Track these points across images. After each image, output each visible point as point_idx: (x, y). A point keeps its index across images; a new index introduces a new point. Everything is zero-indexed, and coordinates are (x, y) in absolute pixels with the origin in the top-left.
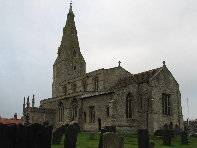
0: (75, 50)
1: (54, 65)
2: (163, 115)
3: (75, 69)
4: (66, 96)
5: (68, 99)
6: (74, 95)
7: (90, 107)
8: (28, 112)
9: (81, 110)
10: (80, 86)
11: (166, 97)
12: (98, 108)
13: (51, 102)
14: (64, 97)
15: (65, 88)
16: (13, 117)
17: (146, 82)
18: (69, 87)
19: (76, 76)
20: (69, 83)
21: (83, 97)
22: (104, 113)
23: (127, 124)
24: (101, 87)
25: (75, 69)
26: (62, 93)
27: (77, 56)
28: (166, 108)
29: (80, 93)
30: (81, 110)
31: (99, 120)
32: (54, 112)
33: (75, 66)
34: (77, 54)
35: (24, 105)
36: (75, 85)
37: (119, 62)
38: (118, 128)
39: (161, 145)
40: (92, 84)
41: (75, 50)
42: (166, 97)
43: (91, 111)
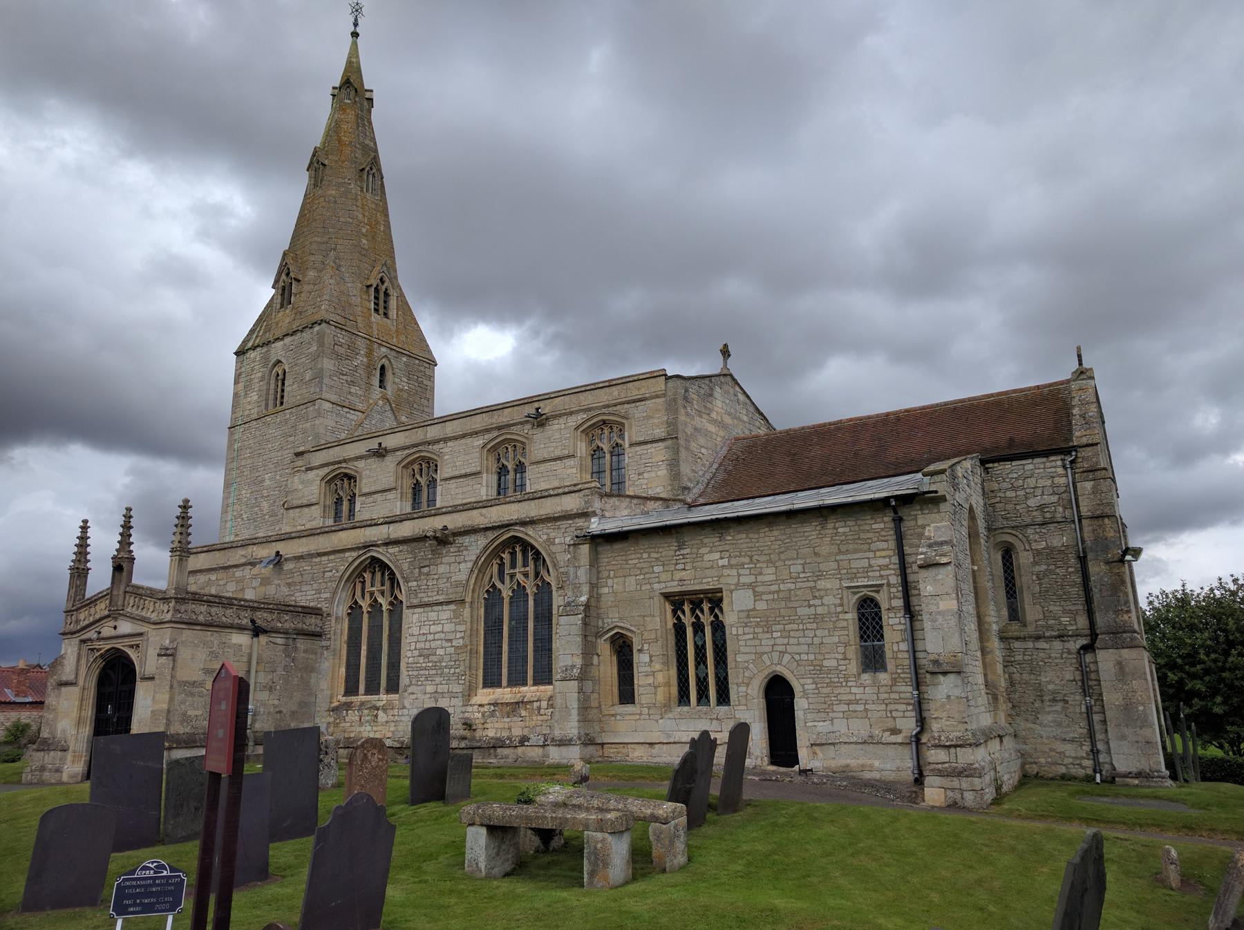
0: (382, 281)
1: (240, 353)
2: (683, 697)
3: (382, 384)
4: (436, 523)
5: (443, 540)
6: (497, 514)
7: (667, 596)
8: (125, 627)
10: (663, 435)
11: (696, 605)
12: (761, 606)
13: (278, 560)
14: (406, 530)
15: (342, 482)
18: (377, 475)
19: (390, 423)
20: (380, 453)
21: (595, 526)
24: (648, 472)
25: (382, 384)
26: (316, 511)
29: (571, 503)
31: (779, 694)
32: (312, 623)
33: (383, 368)
35: (80, 571)
36: (430, 464)
37: (725, 352)
38: (477, 759)
40: (571, 462)
41: (382, 281)
42: (696, 605)
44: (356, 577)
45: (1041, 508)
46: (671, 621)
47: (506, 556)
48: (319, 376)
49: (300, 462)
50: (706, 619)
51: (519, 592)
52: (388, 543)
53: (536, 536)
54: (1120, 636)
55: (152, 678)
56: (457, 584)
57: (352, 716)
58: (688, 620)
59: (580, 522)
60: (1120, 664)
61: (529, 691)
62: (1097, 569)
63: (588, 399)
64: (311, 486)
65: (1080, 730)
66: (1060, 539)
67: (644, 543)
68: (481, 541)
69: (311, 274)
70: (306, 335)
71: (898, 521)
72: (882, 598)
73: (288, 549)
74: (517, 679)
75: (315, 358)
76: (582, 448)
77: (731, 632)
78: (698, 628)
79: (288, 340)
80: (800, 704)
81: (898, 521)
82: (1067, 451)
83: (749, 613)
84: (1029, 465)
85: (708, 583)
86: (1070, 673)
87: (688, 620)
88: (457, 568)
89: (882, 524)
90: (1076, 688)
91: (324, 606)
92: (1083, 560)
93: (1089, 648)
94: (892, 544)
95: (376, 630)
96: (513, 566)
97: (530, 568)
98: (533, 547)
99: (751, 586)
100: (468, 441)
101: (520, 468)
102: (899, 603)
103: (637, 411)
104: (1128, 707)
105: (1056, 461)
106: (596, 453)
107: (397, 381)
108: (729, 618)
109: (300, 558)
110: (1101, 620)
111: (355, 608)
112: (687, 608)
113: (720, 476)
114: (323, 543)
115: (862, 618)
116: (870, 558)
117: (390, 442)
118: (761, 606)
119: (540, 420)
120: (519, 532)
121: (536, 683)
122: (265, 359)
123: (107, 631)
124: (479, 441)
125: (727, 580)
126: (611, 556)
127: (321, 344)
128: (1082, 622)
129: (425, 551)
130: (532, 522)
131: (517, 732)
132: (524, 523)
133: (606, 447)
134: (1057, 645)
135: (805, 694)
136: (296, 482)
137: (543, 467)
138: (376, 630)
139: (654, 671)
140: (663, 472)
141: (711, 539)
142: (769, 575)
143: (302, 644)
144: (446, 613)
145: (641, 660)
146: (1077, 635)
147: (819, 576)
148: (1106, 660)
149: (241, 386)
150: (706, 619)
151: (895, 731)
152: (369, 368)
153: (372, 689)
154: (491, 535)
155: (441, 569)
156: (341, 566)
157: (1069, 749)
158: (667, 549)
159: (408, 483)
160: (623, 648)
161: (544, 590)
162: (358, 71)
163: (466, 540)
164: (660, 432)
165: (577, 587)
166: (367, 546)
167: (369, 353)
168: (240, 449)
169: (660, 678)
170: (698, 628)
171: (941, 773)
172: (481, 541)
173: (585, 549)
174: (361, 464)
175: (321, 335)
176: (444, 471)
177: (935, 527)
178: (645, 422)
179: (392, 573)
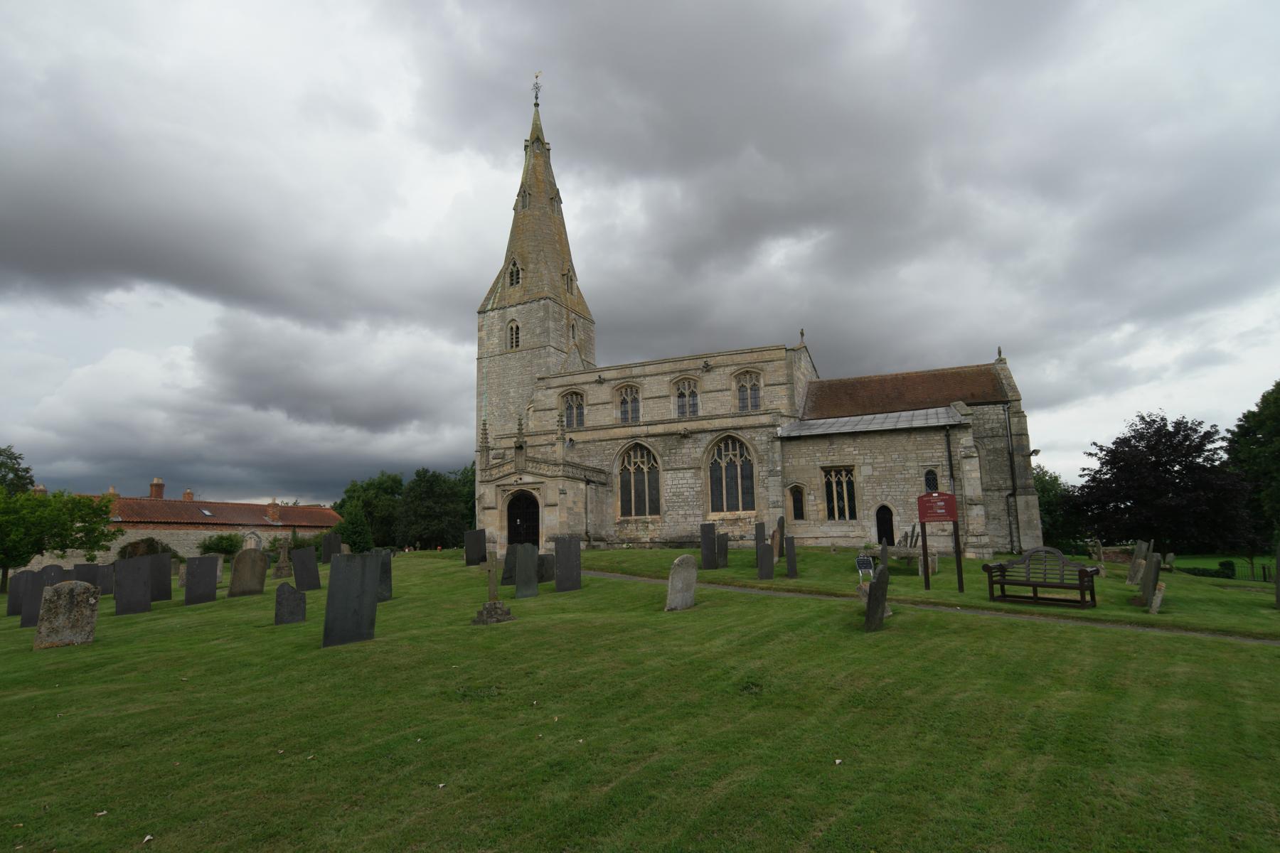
2: (831, 515)
6: (729, 423)
7: (822, 468)
8: (528, 479)
11: (838, 472)
12: (876, 473)
15: (574, 399)
20: (601, 381)
32: (602, 478)
42: (838, 472)
44: (627, 453)
45: (992, 429)
46: (824, 480)
47: (722, 445)
48: (546, 332)
49: (541, 383)
50: (844, 479)
51: (731, 464)
52: (648, 436)
53: (744, 436)
54: (1026, 490)
55: (555, 505)
56: (696, 459)
57: (631, 527)
58: (834, 480)
59: (771, 430)
60: (1027, 502)
61: (741, 513)
62: (1018, 459)
63: (738, 359)
64: (551, 398)
65: (1005, 532)
66: (1001, 444)
67: (811, 442)
69: (531, 266)
70: (535, 305)
71: (948, 436)
72: (939, 472)
75: (543, 320)
76: (734, 385)
78: (839, 483)
79: (519, 307)
80: (896, 519)
81: (948, 436)
82: (1006, 403)
83: (869, 477)
84: (986, 408)
85: (847, 462)
86: (1002, 506)
87: (834, 480)
88: (696, 451)
89: (940, 437)
90: (1004, 513)
91: (606, 469)
92: (1011, 455)
93: (1013, 495)
94: (944, 446)
95: (639, 482)
96: (727, 450)
97: (738, 452)
98: (739, 441)
101: (693, 394)
102: (947, 473)
103: (769, 367)
104: (1029, 522)
105: (1000, 407)
106: (742, 389)
107: (580, 335)
108: (858, 478)
109: (584, 442)
110: (1019, 482)
111: (624, 471)
112: (844, 473)
113: (810, 404)
115: (927, 480)
116: (935, 453)
117: (606, 375)
118: (876, 473)
119: (708, 368)
120: (733, 433)
121: (744, 509)
122: (503, 318)
124: (667, 378)
125: (860, 459)
126: (793, 447)
127: (547, 311)
128: (1009, 483)
129: (672, 441)
130: (741, 428)
131: (737, 533)
132: (736, 429)
133: (748, 386)
134: (997, 493)
135: (899, 514)
136: (539, 395)
137: (710, 395)
138: (639, 482)
139: (815, 503)
140: (785, 401)
141: (849, 441)
142: (880, 459)
143: (601, 489)
144: (689, 474)
146: (1006, 489)
148: (1021, 500)
149: (484, 333)
150: (844, 479)
151: (944, 530)
152: (568, 325)
153: (640, 512)
154: (715, 435)
155: (684, 451)
157: (1001, 541)
158: (824, 445)
159: (618, 400)
162: (541, 130)
163: (699, 436)
164: (782, 379)
165: (774, 463)
166: (633, 437)
167: (568, 318)
168: (488, 372)
169: (821, 507)
170: (839, 483)
171: (974, 547)
172: (709, 437)
173: (778, 443)
174: (586, 387)
175: (546, 308)
177: (966, 439)
178: (773, 373)
179: (649, 452)
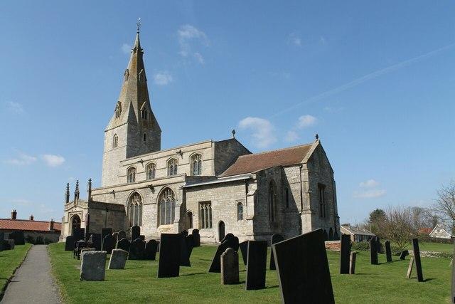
7: (200, 202)
8: (78, 209)
9: (183, 207)
12: (219, 205)
13: (113, 192)
16: (10, 216)
17: (296, 165)
22: (234, 212)
23: (270, 231)
27: (148, 118)
28: (321, 205)
30: (183, 207)
34: (148, 114)
37: (234, 132)
39: (154, 276)
43: (321, 205)
68: (160, 188)
73: (116, 189)
74: (168, 223)
77: (213, 211)
78: (206, 210)
80: (226, 227)
82: (299, 165)
99: (217, 200)
100: (163, 159)
114: (124, 188)
120: (168, 186)
123: (74, 210)
136: (120, 170)
145: (194, 218)
147: (231, 197)
153: (207, 227)
156: (128, 194)
160: (190, 214)
161: (174, 200)
166: (134, 189)
176: (157, 167)
